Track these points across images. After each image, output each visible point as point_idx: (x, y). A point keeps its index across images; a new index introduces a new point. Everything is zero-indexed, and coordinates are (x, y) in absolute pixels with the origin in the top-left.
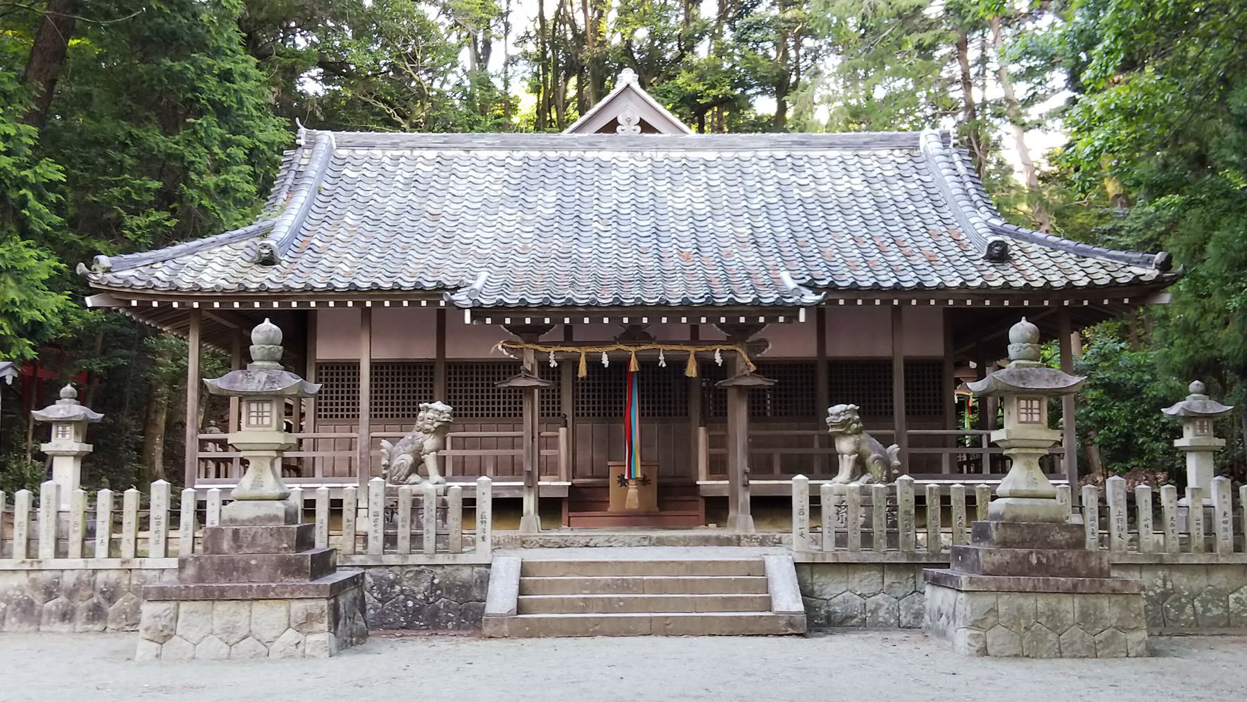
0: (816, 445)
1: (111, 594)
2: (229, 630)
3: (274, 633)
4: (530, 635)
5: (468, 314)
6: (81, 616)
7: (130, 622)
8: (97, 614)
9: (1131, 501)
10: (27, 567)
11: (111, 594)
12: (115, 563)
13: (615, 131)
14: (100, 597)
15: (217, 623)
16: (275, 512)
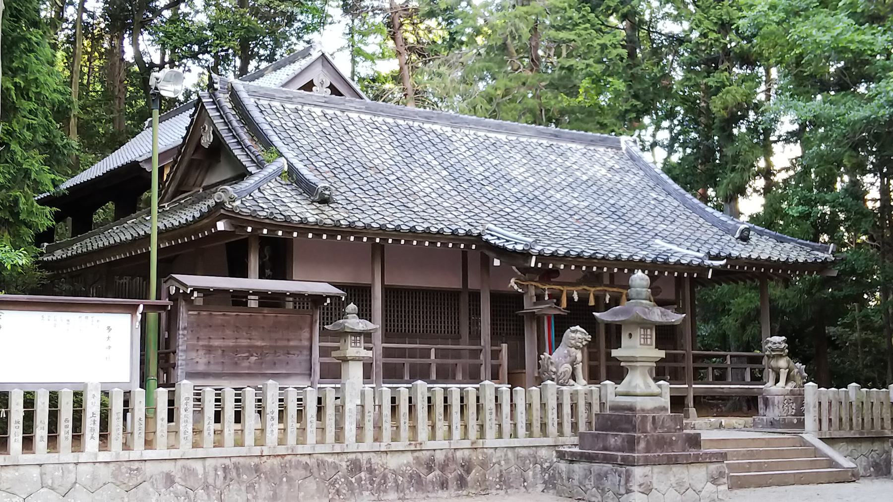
0: (433, 356)
1: (467, 467)
2: (680, 484)
3: (702, 485)
4: (741, 487)
5: (534, 258)
6: (453, 485)
7: (483, 488)
8: (462, 483)
9: (198, 398)
10: (413, 448)
11: (467, 467)
12: (467, 444)
13: (311, 90)
14: (461, 469)
15: (673, 480)
16: (663, 404)
